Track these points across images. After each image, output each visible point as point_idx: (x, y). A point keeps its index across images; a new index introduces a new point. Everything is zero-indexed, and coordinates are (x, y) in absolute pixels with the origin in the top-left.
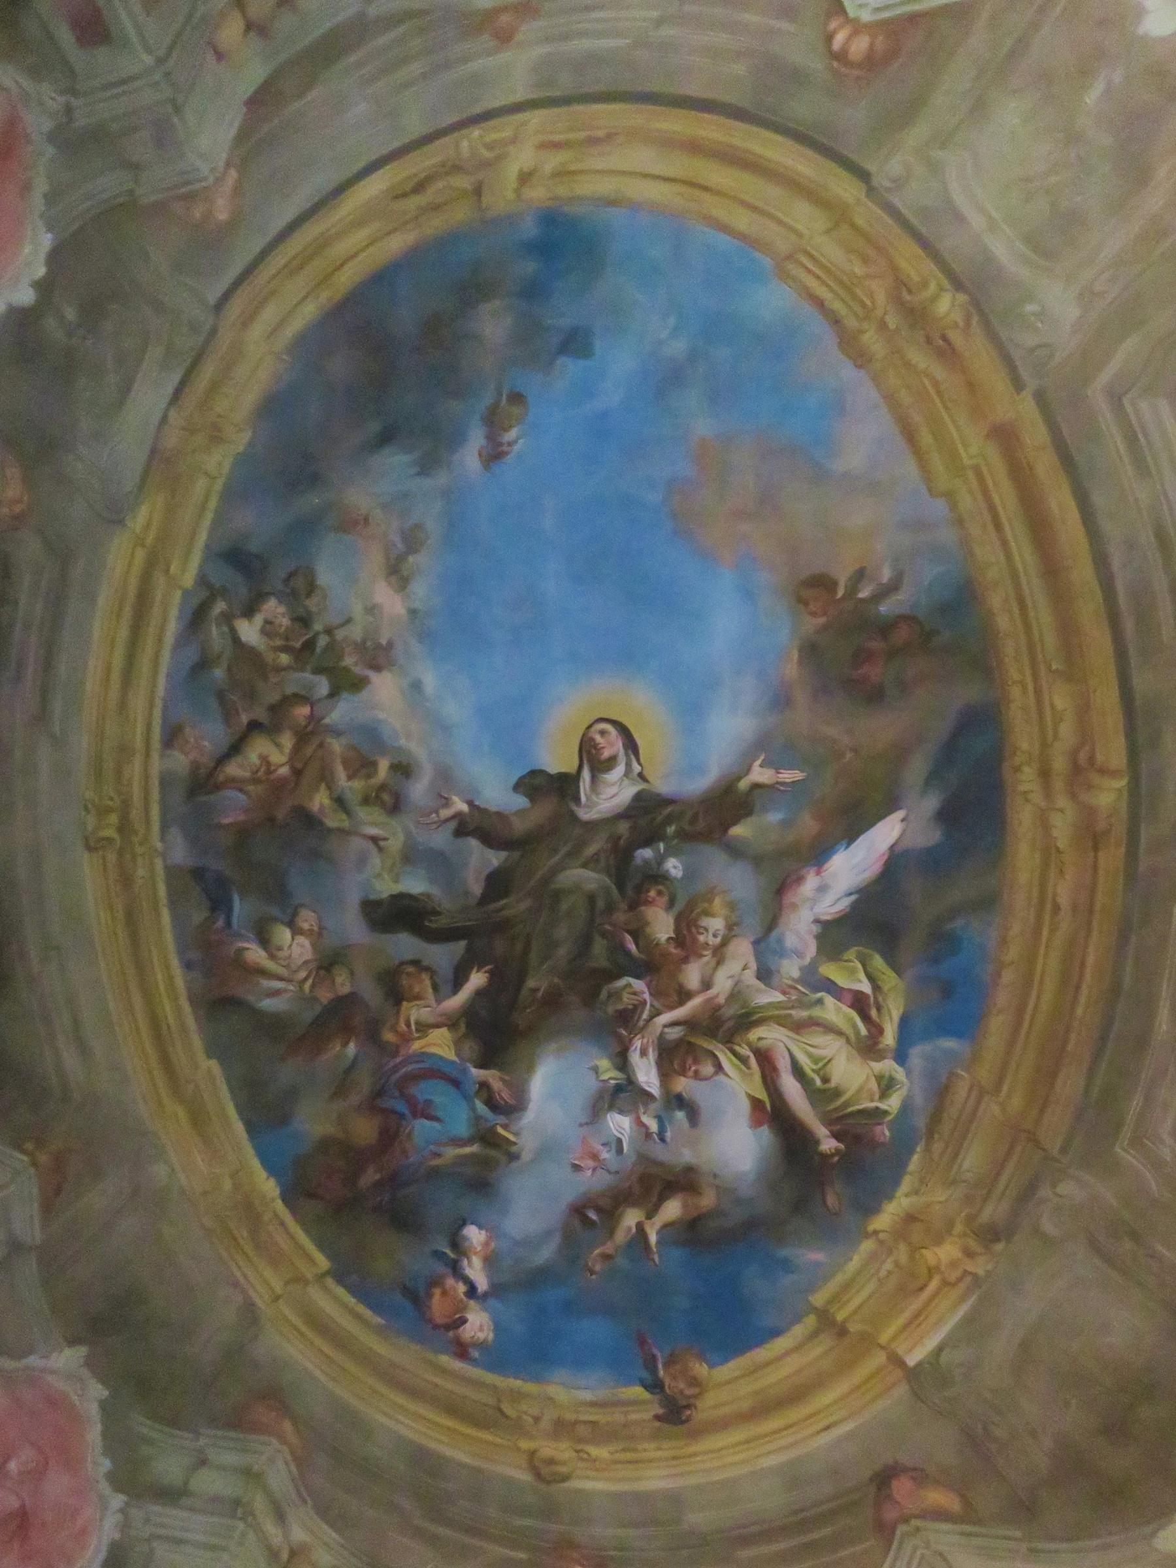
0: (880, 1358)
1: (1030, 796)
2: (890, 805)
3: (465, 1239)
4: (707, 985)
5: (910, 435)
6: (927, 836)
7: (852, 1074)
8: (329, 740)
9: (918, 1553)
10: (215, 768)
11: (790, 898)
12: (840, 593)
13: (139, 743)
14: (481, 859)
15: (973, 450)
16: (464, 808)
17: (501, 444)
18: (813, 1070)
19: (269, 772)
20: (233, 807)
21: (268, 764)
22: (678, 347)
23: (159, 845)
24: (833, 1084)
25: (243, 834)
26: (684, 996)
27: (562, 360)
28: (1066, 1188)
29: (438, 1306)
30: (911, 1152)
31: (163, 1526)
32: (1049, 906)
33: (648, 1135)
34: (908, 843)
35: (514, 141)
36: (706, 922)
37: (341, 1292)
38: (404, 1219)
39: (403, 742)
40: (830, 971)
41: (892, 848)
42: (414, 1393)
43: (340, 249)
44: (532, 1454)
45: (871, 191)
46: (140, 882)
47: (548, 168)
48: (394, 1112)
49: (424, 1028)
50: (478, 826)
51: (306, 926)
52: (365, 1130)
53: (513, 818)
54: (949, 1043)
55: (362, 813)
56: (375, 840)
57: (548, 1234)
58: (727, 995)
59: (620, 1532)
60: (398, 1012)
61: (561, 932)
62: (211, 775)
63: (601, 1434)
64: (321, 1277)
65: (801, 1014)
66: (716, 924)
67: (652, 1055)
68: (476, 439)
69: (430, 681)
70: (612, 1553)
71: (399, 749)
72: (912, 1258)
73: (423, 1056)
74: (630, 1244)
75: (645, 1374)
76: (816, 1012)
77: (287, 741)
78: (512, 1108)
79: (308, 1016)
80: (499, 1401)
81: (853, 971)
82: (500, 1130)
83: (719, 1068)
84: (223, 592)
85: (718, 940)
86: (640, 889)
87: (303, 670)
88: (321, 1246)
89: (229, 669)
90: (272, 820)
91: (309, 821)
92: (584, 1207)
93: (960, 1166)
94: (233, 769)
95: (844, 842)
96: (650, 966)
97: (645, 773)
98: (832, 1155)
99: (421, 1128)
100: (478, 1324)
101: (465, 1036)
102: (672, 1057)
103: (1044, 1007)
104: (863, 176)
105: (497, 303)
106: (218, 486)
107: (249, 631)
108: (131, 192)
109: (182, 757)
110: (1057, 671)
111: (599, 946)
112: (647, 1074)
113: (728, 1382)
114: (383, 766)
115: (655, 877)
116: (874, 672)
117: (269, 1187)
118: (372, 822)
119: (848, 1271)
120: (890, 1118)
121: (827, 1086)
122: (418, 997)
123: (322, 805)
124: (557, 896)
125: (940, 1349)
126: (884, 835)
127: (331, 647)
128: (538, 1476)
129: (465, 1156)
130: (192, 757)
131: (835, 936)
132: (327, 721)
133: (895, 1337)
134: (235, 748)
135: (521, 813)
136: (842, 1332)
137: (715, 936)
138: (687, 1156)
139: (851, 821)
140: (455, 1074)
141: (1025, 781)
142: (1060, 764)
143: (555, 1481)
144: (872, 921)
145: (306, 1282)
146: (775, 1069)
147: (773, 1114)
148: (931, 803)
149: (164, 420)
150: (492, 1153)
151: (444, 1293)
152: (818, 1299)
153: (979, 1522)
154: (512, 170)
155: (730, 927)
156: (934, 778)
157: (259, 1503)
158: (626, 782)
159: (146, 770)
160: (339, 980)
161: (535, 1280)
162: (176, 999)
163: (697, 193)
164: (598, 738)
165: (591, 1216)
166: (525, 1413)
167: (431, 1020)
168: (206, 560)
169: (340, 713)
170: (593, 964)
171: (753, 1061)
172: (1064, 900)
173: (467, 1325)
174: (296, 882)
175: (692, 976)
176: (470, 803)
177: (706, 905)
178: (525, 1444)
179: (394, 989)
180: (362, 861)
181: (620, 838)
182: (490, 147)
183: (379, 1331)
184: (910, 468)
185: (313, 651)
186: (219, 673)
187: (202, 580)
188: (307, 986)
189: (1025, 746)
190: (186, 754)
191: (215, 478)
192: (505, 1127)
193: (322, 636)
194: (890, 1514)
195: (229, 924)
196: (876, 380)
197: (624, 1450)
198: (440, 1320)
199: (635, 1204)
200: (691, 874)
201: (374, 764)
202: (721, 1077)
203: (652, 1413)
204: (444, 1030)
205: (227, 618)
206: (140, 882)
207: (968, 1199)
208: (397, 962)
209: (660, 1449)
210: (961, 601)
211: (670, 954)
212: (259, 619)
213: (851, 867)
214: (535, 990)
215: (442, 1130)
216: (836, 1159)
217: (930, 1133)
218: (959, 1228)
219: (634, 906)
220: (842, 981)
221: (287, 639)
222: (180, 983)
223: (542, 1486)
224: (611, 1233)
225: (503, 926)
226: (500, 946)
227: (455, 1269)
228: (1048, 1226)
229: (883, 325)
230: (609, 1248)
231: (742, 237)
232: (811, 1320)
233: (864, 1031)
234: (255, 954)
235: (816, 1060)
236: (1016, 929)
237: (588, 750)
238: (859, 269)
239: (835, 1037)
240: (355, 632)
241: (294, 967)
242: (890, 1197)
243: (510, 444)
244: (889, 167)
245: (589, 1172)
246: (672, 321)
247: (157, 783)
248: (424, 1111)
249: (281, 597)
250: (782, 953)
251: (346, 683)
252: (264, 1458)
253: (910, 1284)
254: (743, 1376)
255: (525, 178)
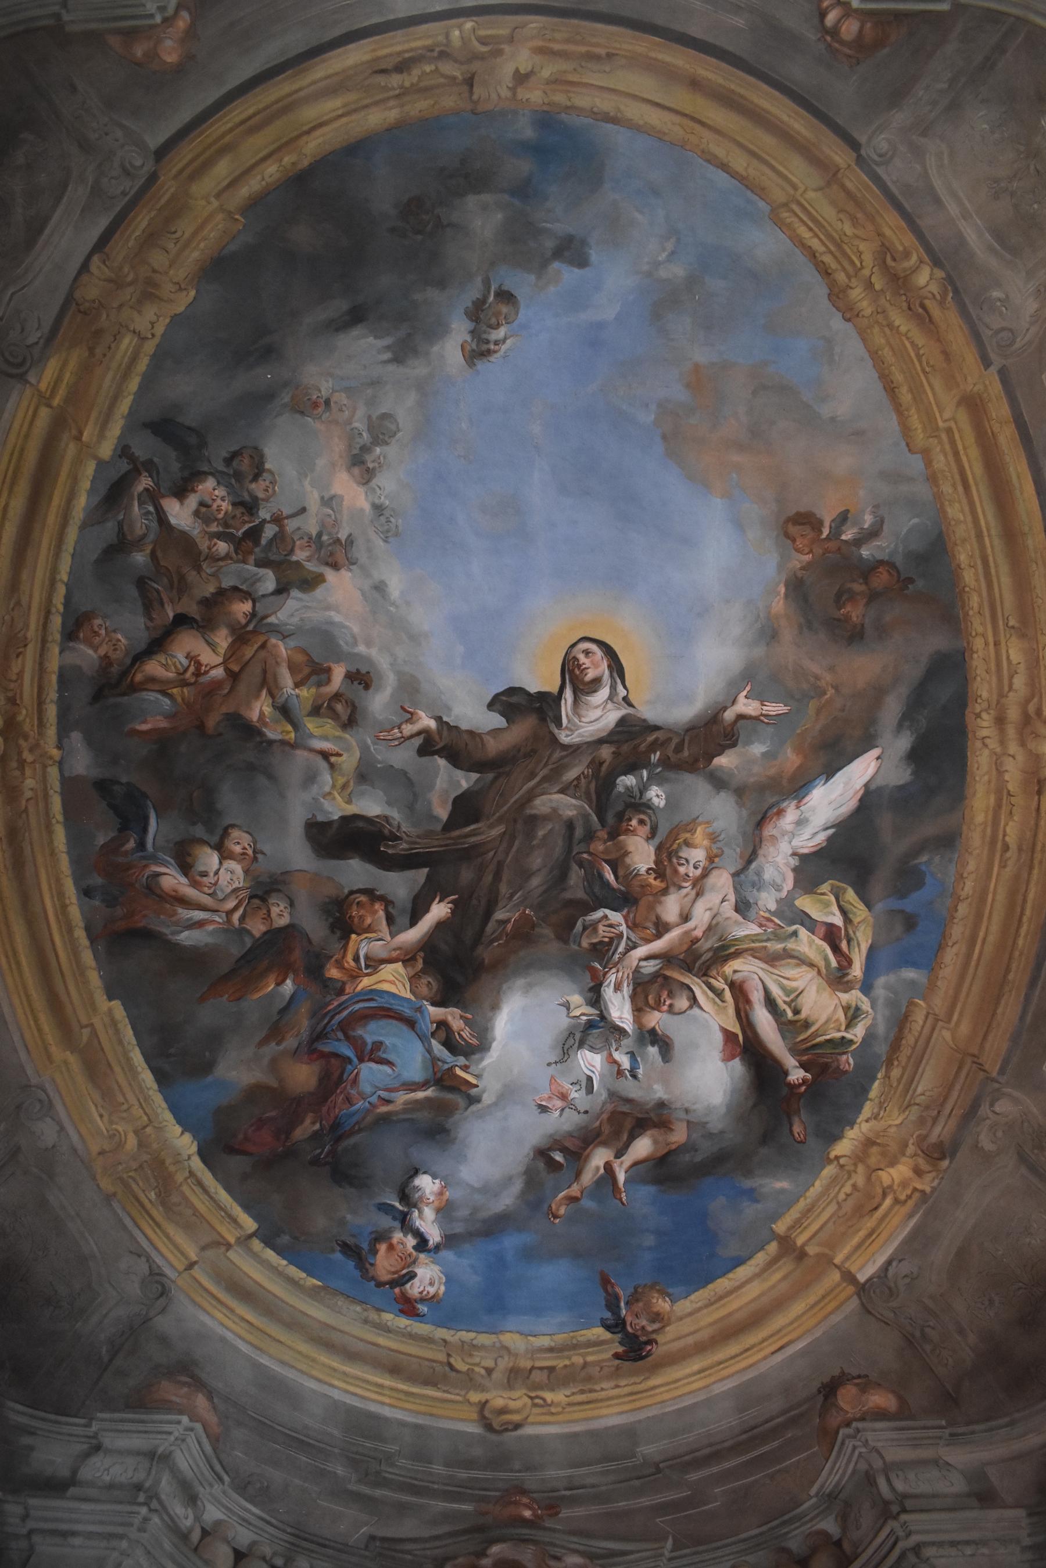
0: (836, 1276)
1: (987, 741)
2: (866, 743)
3: (417, 1189)
4: (685, 918)
5: (891, 390)
6: (899, 775)
7: (821, 1005)
8: (273, 641)
9: (857, 1453)
10: (133, 664)
11: (769, 830)
12: (826, 532)
13: (32, 632)
14: (448, 782)
15: (947, 415)
16: (432, 724)
17: (488, 342)
18: (785, 1002)
19: (198, 674)
20: (154, 712)
21: (198, 664)
22: (677, 271)
23: (55, 753)
24: (803, 1015)
25: (163, 744)
26: (662, 928)
27: (556, 265)
28: (1003, 1106)
29: (384, 1264)
30: (874, 1078)
31: (46, 1520)
32: (999, 845)
33: (620, 1073)
34: (879, 782)
35: (511, 40)
36: (684, 853)
37: (270, 1254)
38: (345, 1171)
39: (361, 649)
40: (805, 903)
41: (866, 785)
42: (351, 1356)
43: (310, 113)
44: (483, 1405)
45: (860, 160)
46: (28, 794)
47: (546, 73)
48: (336, 1055)
49: (374, 963)
50: (447, 744)
51: (238, 849)
52: (303, 1076)
53: (487, 738)
54: (910, 974)
55: (311, 725)
56: (325, 755)
57: (509, 1179)
58: (704, 928)
59: (569, 1472)
60: (345, 948)
61: (536, 861)
62: (124, 674)
63: (555, 1378)
64: (244, 1241)
65: (777, 946)
66: (697, 855)
67: (626, 990)
68: (459, 330)
69: (395, 587)
70: (564, 1493)
71: (358, 655)
72: (869, 1178)
73: (371, 994)
74: (599, 1183)
75: (608, 1315)
76: (791, 945)
77: (223, 639)
78: (471, 1050)
79: (236, 951)
80: (449, 1355)
81: (827, 905)
82: (459, 1072)
83: (694, 1001)
84: (149, 466)
85: (699, 872)
86: (620, 817)
87: (244, 561)
88: (246, 1208)
89: (153, 553)
90: (201, 727)
91: (249, 731)
92: (550, 1149)
93: (915, 1090)
94: (154, 667)
95: (824, 777)
96: (627, 898)
97: (631, 697)
98: (800, 1085)
99: (370, 1074)
100: (428, 1277)
101: (423, 971)
102: (647, 991)
103: (991, 938)
104: (854, 145)
105: (486, 197)
106: (150, 347)
107: (180, 514)
108: (57, 16)
109: (91, 652)
110: (1013, 627)
111: (576, 875)
112: (620, 1009)
113: (691, 1314)
114: (339, 673)
115: (637, 805)
116: (855, 612)
117: (186, 1144)
118: (322, 733)
119: (807, 1198)
120: (854, 1047)
121: (796, 1018)
122: (369, 929)
123: (262, 713)
124: (533, 821)
125: (889, 1263)
126: (860, 772)
127: (280, 537)
128: (489, 1427)
129: (417, 1101)
130: (102, 651)
131: (811, 870)
132: (272, 619)
133: (847, 1258)
134: (157, 645)
135: (495, 732)
136: (802, 1255)
137: (696, 868)
138: (659, 1092)
139: (831, 755)
140: (408, 1012)
141: (983, 726)
142: (1013, 714)
143: (507, 1430)
144: (847, 856)
145: (229, 1246)
146: (748, 1001)
147: (745, 1046)
148: (904, 743)
149: (85, 267)
150: (449, 1096)
151: (391, 1247)
152: (780, 1227)
153: (912, 1417)
154: (507, 69)
155: (711, 859)
156: (907, 718)
157: (166, 1485)
158: (610, 705)
159: (41, 664)
160: (275, 910)
161: (493, 1227)
162: (70, 930)
163: (697, 126)
164: (582, 658)
165: (556, 1158)
166: (477, 1365)
167: (384, 955)
168: (129, 429)
169: (292, 611)
170: (568, 895)
171: (728, 994)
172: (1012, 839)
173: (416, 1281)
174: (228, 798)
175: (670, 908)
176: (439, 719)
177: (688, 835)
178: (475, 1397)
179: (341, 920)
180: (310, 778)
181: (601, 764)
182: (483, 41)
183: (313, 1293)
184: (892, 423)
185: (257, 542)
186: (140, 558)
187: (124, 451)
188: (236, 916)
189: (985, 694)
190: (96, 649)
191: (145, 339)
192: (465, 1068)
193: (267, 525)
194: (834, 1420)
195: (141, 845)
196: (863, 335)
197: (582, 1392)
198: (385, 1277)
199: (605, 1144)
200: (672, 803)
201: (329, 671)
202: (696, 1011)
203: (612, 1352)
204: (399, 966)
205: (153, 496)
206: (28, 794)
207: (921, 1121)
208: (346, 891)
209: (617, 1386)
210: (933, 554)
211: (650, 885)
212: (192, 501)
213: (830, 800)
214: (504, 922)
215: (396, 1069)
216: (803, 1088)
217: (889, 1063)
218: (911, 1149)
219: (614, 834)
220: (816, 914)
221: (226, 525)
222: (75, 912)
223: (493, 1437)
224: (578, 1175)
225: (469, 854)
226: (466, 875)
227: (404, 1222)
228: (986, 1143)
229: (869, 285)
230: (575, 1190)
231: (742, 179)
232: (773, 1247)
233: (834, 963)
234: (172, 880)
235: (787, 991)
236: (972, 866)
237: (570, 669)
238: (848, 228)
239: (808, 969)
240: (312, 527)
241: (220, 895)
242: (852, 1124)
243: (496, 343)
244: (879, 142)
245: (557, 1113)
246: (670, 246)
247: (54, 678)
248: (374, 1054)
249: (221, 478)
250: (758, 885)
251: (295, 580)
252: (172, 1438)
253: (866, 1205)
254: (706, 1306)
255: (521, 78)
